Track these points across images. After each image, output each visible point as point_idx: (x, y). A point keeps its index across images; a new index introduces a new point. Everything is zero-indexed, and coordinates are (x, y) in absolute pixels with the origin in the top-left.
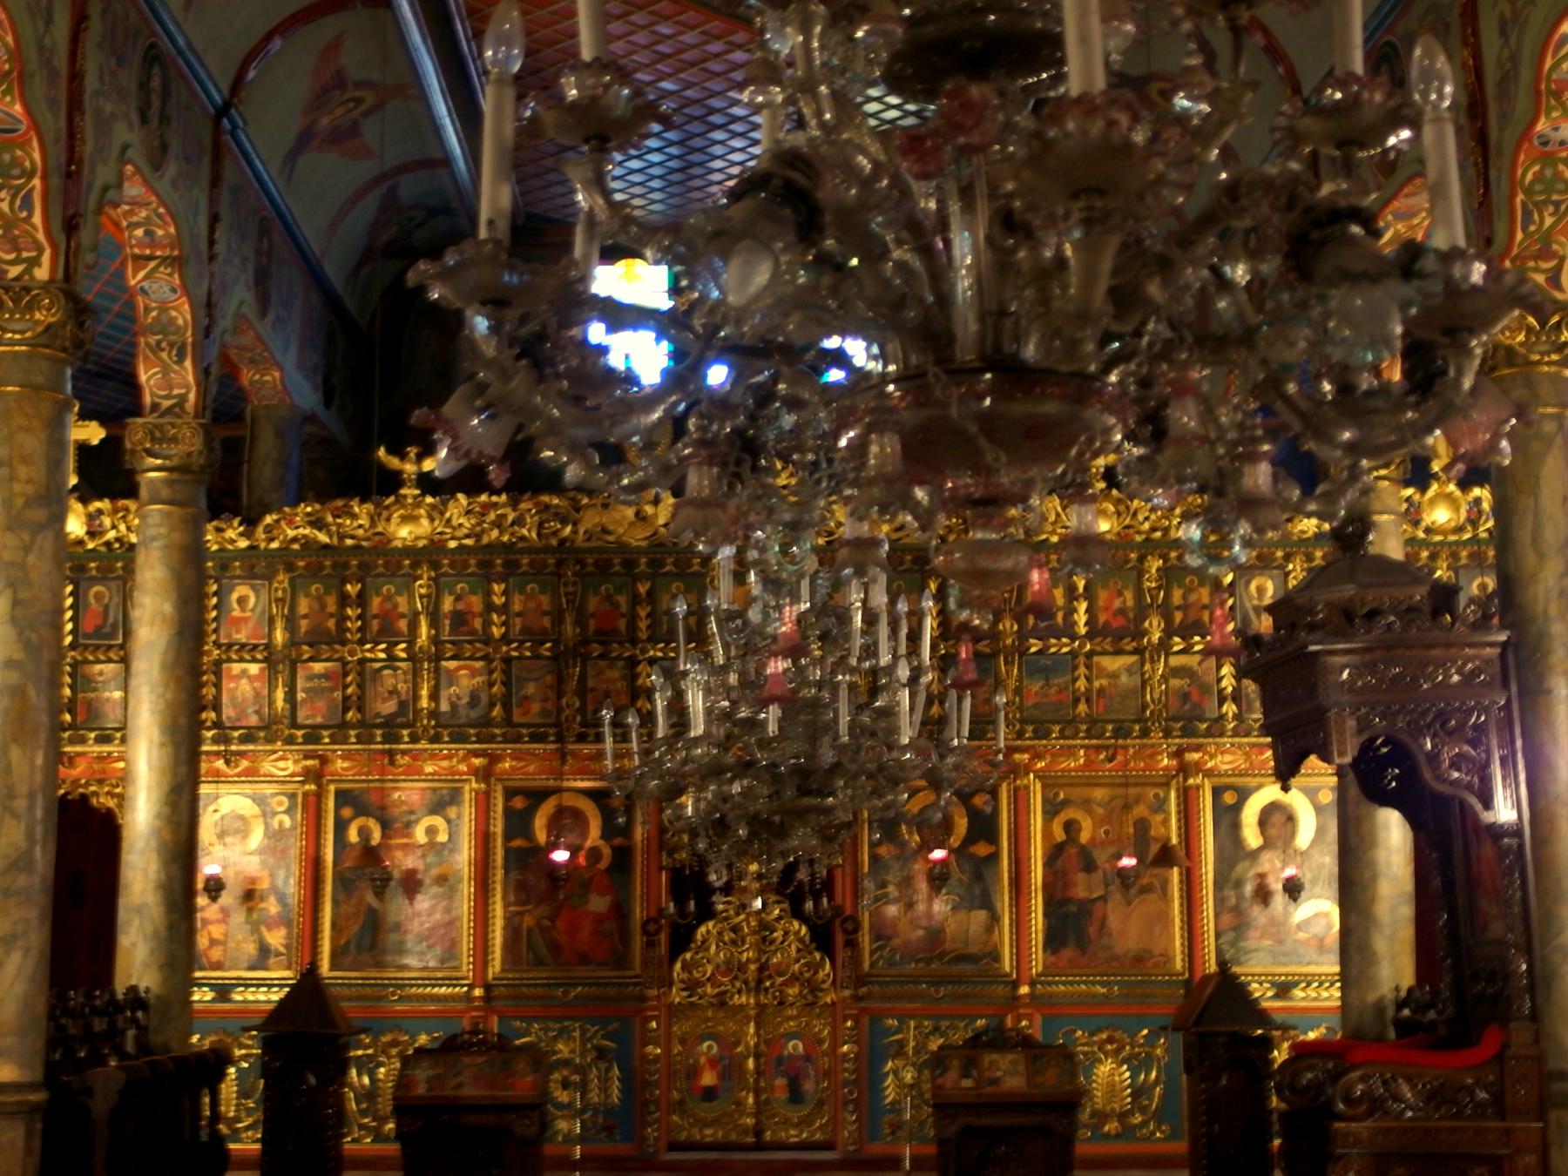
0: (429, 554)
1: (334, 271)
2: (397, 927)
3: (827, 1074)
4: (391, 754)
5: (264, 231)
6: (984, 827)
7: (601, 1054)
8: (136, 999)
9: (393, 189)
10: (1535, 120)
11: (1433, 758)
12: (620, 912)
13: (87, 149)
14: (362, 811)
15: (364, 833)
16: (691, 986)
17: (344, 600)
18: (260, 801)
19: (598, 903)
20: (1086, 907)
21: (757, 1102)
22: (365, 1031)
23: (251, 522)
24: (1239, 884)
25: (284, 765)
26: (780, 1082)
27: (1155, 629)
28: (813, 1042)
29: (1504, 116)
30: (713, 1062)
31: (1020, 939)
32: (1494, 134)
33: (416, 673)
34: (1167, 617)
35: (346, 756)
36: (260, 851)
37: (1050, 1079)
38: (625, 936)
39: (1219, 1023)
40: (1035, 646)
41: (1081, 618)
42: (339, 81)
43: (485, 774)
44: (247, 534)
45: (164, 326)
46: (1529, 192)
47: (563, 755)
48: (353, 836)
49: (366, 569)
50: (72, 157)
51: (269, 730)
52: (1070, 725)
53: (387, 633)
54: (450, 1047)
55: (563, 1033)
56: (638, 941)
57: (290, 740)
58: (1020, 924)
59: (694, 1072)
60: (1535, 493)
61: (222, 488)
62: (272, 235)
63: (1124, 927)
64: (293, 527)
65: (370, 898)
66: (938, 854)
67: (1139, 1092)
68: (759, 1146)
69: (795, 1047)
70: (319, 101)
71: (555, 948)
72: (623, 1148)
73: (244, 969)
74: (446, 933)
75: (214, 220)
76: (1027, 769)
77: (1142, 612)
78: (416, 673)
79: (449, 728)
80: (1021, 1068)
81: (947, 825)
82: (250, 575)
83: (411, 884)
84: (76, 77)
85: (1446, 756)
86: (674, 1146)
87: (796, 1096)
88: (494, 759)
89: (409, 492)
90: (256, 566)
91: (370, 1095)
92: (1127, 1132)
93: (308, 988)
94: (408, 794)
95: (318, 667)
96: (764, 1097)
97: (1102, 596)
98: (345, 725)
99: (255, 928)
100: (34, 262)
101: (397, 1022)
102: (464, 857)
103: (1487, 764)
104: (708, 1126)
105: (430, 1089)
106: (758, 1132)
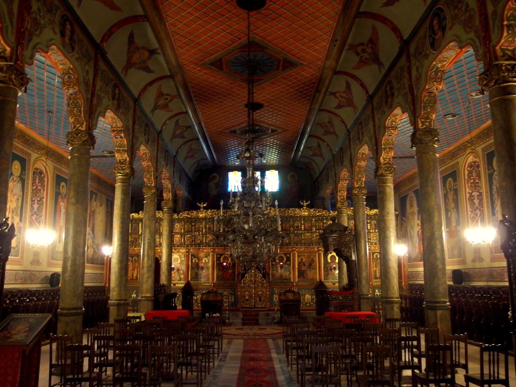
0: (205, 219)
1: (190, 175)
2: (200, 275)
3: (265, 297)
4: (199, 249)
5: (180, 171)
6: (288, 259)
7: (231, 294)
8: (164, 286)
9: (199, 163)
10: (425, 86)
11: (344, 251)
12: (234, 272)
13: (158, 167)
14: (195, 257)
15: (195, 261)
16: (244, 284)
17: (192, 226)
18: (180, 256)
19: (230, 271)
20: (304, 271)
22: (196, 290)
23: (178, 214)
24: (327, 268)
25: (183, 250)
27: (314, 229)
28: (263, 292)
29: (379, 134)
30: (248, 295)
31: (294, 277)
32: (415, 92)
33: (203, 237)
34: (316, 228)
35: (193, 249)
36: (180, 263)
37: (297, 297)
38: (235, 277)
39: (320, 289)
40: (296, 232)
41: (303, 228)
42: (192, 150)
43: (213, 252)
44: (178, 216)
45: (167, 188)
46: (425, 103)
47: (225, 249)
48: (194, 261)
49: (195, 221)
50: (157, 169)
51: (181, 245)
52: (301, 244)
53: (199, 230)
54: (209, 293)
55: (225, 291)
56: (236, 277)
57: (184, 247)
58: (294, 274)
59: (245, 297)
60: (359, 213)
61: (175, 210)
62: (182, 171)
63: (310, 274)
64: (185, 215)
65: (196, 271)
66: (281, 263)
67: (312, 299)
68: (255, 308)
69: (260, 293)
70: (188, 153)
71: (224, 278)
72: (235, 308)
73: (179, 283)
74: (208, 277)
75: (174, 172)
76: (295, 250)
77: (312, 226)
78: (203, 237)
79: (208, 245)
81: (283, 259)
82: (178, 222)
83: (202, 268)
84: (157, 157)
85: (346, 251)
86: (242, 308)
87: (260, 300)
88: (215, 249)
89: (202, 209)
90: (179, 220)
91: (197, 300)
92: (310, 305)
93: (188, 285)
94: (202, 255)
95: (188, 236)
97: (306, 224)
98: (192, 244)
99: (179, 275)
100: (152, 184)
101: (200, 289)
102: (210, 264)
103: (351, 252)
106: (255, 306)
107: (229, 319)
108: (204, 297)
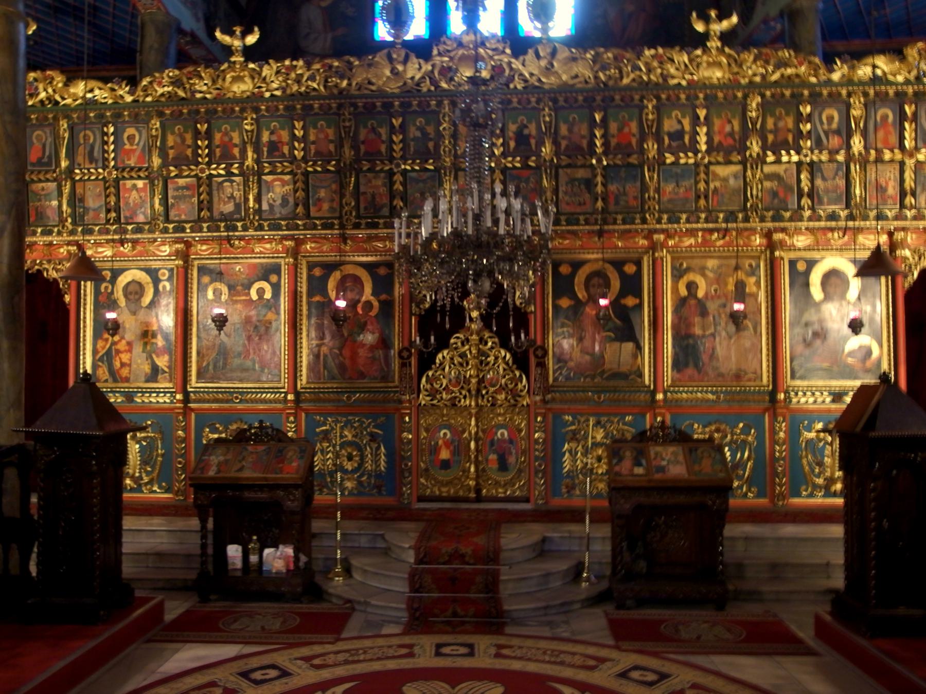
26: (493, 457)
68: (479, 499)
80: (681, 458)
105: (219, 471)
106: (478, 491)
107: (348, 571)
108: (215, 459)
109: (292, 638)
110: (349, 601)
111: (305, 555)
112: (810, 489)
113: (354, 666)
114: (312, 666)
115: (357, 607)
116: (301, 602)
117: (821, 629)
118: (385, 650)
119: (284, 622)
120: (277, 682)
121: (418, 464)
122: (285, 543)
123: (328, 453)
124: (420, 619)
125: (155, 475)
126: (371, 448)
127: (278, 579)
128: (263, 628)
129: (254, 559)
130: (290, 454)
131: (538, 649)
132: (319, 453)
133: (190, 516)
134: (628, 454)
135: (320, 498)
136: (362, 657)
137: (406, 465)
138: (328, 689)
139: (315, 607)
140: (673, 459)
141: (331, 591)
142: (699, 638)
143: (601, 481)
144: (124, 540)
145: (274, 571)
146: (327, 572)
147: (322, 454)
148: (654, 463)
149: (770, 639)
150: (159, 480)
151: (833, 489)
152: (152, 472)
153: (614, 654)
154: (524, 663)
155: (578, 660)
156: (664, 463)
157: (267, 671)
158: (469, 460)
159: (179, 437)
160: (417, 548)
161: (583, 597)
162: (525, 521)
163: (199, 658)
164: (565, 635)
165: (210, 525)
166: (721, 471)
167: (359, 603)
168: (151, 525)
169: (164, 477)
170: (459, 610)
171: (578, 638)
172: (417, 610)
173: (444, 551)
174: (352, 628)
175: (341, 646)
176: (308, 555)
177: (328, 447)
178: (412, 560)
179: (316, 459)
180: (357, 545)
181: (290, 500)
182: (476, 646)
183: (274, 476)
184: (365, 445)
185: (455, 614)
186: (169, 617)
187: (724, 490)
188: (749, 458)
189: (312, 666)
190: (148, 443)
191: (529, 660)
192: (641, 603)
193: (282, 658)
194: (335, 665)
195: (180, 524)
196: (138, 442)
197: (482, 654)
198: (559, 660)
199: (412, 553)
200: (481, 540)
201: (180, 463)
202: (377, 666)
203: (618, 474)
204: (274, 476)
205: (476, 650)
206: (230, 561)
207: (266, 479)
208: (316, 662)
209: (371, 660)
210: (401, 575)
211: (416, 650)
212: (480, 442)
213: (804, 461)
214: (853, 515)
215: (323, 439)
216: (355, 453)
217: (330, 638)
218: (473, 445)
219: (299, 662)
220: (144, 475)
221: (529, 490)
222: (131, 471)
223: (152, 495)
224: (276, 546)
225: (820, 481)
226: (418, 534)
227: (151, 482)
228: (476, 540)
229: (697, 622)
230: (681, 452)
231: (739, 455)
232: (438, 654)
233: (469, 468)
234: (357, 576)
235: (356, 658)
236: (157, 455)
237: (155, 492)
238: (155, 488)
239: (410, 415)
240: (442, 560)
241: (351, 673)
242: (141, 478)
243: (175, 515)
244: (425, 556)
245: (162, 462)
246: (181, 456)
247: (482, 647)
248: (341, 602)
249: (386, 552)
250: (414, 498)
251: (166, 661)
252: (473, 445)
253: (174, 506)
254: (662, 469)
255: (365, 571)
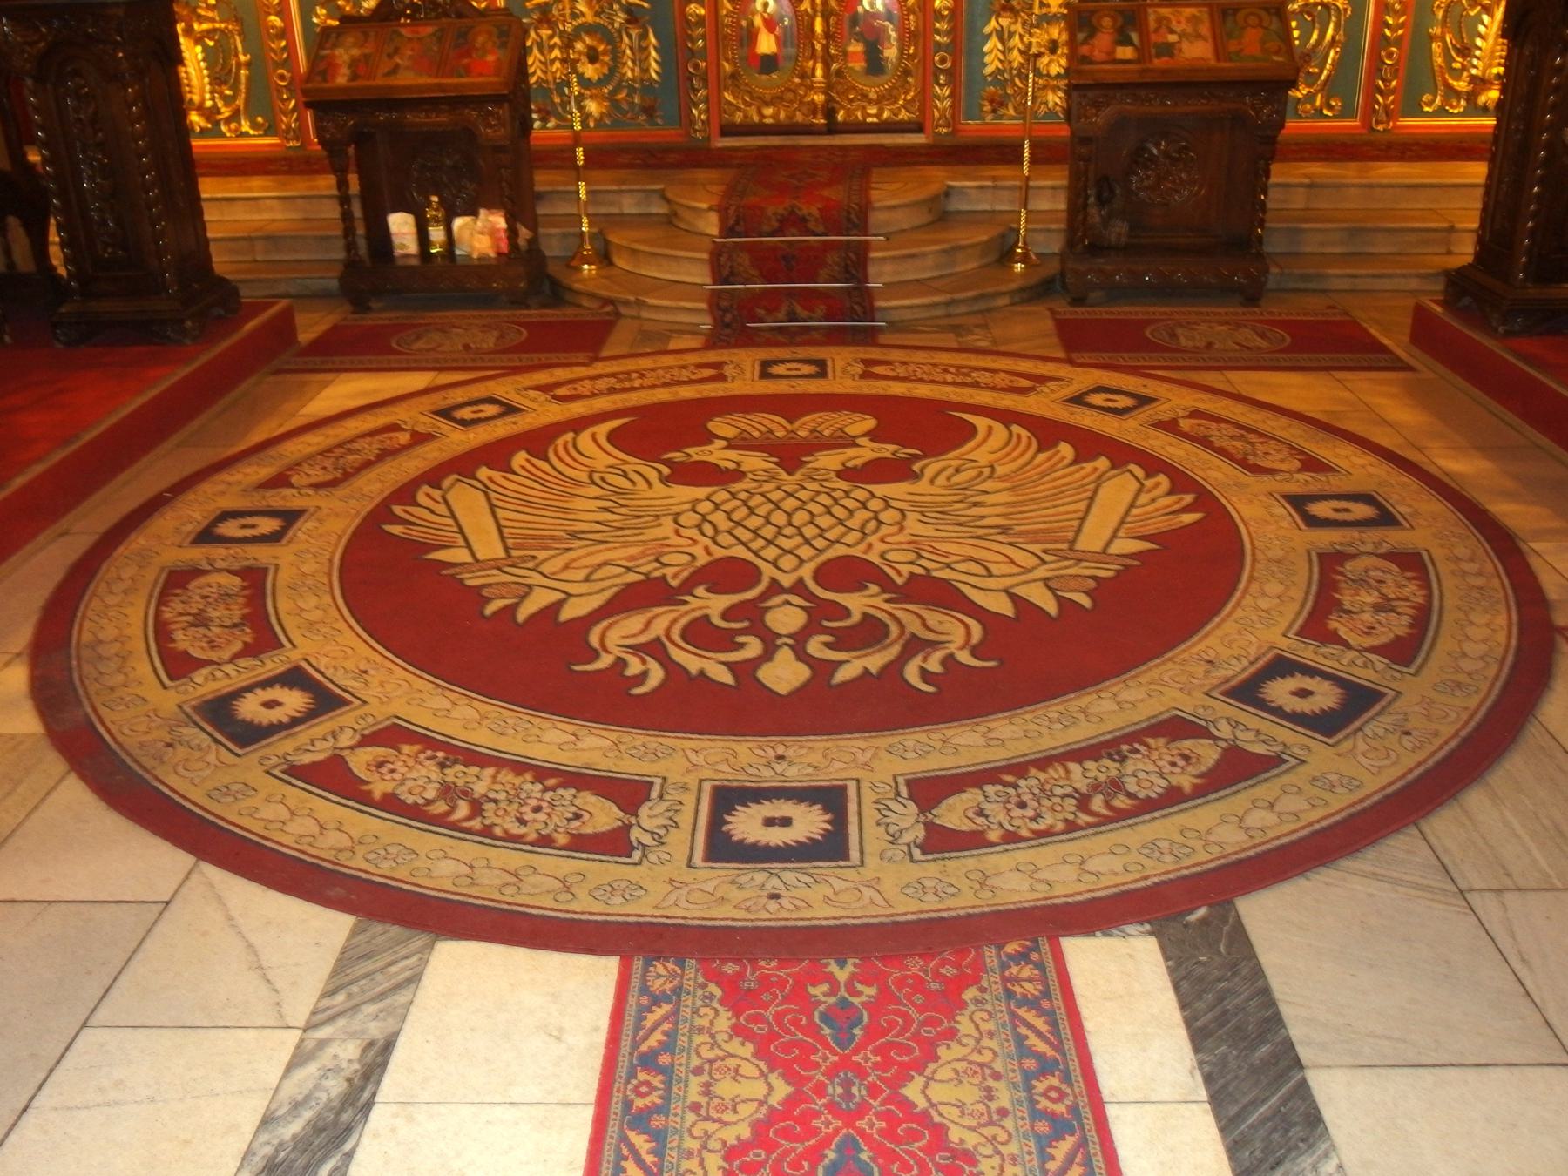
21: (827, 74)
26: (856, 47)
68: (832, 128)
80: (1205, 29)
96: (835, 66)
104: (767, 104)
105: (354, 77)
106: (830, 113)
107: (604, 257)
108: (344, 54)
109: (515, 360)
110: (610, 301)
111: (527, 227)
112: (1438, 101)
113: (625, 396)
114: (554, 397)
115: (623, 310)
116: (528, 307)
117: (1424, 331)
118: (676, 372)
119: (502, 336)
120: (499, 422)
121: (718, 65)
122: (490, 206)
123: (552, 48)
124: (733, 325)
125: (240, 102)
126: (630, 37)
127: (480, 269)
128: (467, 347)
129: (437, 234)
130: (481, 39)
131: (935, 365)
132: (536, 51)
133: (317, 172)
134: (1107, 22)
135: (543, 130)
136: (637, 383)
137: (696, 67)
138: (584, 428)
139: (552, 314)
140: (1189, 30)
141: (577, 286)
142: (1209, 345)
143: (1055, 89)
144: (207, 217)
145: (475, 256)
146: (571, 262)
147: (542, 52)
148: (1154, 38)
149: (1334, 343)
150: (251, 111)
151: (1482, 99)
152: (234, 97)
153: (1064, 371)
154: (910, 385)
155: (1002, 380)
156: (1172, 38)
157: (481, 407)
158: (813, 56)
159: (273, 27)
160: (722, 210)
161: (1013, 286)
162: (915, 164)
163: (365, 394)
164: (983, 344)
165: (354, 186)
166: (1277, 53)
167: (627, 303)
168: (250, 190)
169: (260, 103)
170: (799, 309)
171: (1003, 348)
172: (726, 310)
173: (770, 210)
174: (617, 342)
175: (600, 368)
176: (533, 226)
177: (551, 37)
178: (714, 231)
179: (530, 61)
180: (615, 210)
181: (489, 125)
182: (829, 363)
183: (456, 80)
184: (619, 31)
185: (792, 317)
186: (305, 336)
187: (1275, 88)
188: (1333, 42)
189: (554, 397)
190: (216, 42)
191: (921, 380)
192: (1116, 294)
193: (505, 389)
194: (593, 395)
195: (299, 186)
196: (199, 40)
197: (838, 373)
198: (969, 380)
199: (713, 218)
200: (835, 194)
201: (282, 77)
202: (663, 395)
203: (1086, 60)
204: (456, 80)
205: (830, 370)
206: (396, 241)
207: (440, 87)
208: (561, 391)
209: (654, 386)
210: (698, 255)
211: (728, 371)
212: (832, 20)
213: (1436, 47)
214: (1511, 148)
215: (540, 21)
216: (601, 48)
217: (581, 357)
218: (818, 26)
219: (531, 393)
220: (220, 104)
221: (922, 110)
222: (196, 98)
223: (242, 141)
224: (474, 213)
225: (1462, 85)
226: (723, 187)
227: (235, 117)
228: (826, 193)
229: (1208, 324)
230: (1206, 16)
231: (1315, 36)
232: (765, 375)
233: (814, 69)
234: (621, 262)
235: (627, 385)
236: (239, 65)
237: (246, 134)
238: (246, 127)
239: (703, 37)
240: (766, 228)
241: (620, 405)
242: (215, 110)
243: (289, 172)
244: (737, 222)
245: (249, 78)
246: (283, 64)
247: (840, 364)
248: (594, 305)
249: (670, 220)
250: (715, 128)
251: (312, 399)
252: (818, 26)
253: (285, 159)
254: (1168, 50)
255: (634, 251)
